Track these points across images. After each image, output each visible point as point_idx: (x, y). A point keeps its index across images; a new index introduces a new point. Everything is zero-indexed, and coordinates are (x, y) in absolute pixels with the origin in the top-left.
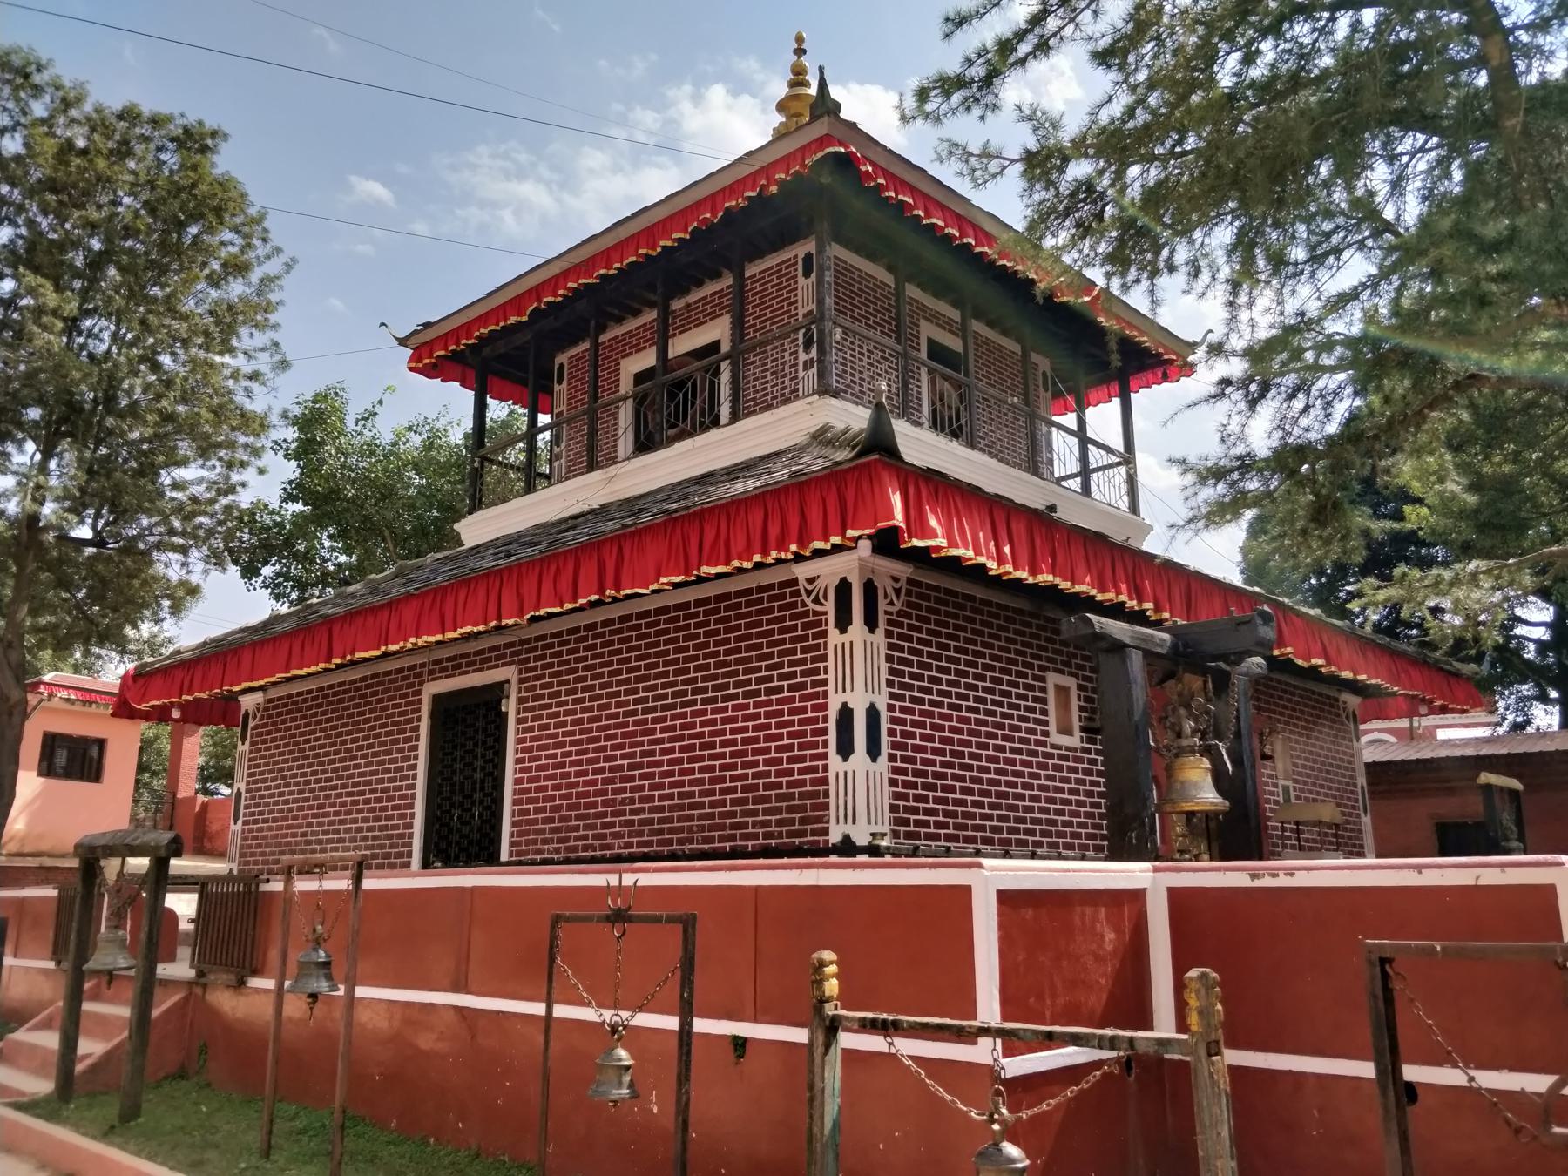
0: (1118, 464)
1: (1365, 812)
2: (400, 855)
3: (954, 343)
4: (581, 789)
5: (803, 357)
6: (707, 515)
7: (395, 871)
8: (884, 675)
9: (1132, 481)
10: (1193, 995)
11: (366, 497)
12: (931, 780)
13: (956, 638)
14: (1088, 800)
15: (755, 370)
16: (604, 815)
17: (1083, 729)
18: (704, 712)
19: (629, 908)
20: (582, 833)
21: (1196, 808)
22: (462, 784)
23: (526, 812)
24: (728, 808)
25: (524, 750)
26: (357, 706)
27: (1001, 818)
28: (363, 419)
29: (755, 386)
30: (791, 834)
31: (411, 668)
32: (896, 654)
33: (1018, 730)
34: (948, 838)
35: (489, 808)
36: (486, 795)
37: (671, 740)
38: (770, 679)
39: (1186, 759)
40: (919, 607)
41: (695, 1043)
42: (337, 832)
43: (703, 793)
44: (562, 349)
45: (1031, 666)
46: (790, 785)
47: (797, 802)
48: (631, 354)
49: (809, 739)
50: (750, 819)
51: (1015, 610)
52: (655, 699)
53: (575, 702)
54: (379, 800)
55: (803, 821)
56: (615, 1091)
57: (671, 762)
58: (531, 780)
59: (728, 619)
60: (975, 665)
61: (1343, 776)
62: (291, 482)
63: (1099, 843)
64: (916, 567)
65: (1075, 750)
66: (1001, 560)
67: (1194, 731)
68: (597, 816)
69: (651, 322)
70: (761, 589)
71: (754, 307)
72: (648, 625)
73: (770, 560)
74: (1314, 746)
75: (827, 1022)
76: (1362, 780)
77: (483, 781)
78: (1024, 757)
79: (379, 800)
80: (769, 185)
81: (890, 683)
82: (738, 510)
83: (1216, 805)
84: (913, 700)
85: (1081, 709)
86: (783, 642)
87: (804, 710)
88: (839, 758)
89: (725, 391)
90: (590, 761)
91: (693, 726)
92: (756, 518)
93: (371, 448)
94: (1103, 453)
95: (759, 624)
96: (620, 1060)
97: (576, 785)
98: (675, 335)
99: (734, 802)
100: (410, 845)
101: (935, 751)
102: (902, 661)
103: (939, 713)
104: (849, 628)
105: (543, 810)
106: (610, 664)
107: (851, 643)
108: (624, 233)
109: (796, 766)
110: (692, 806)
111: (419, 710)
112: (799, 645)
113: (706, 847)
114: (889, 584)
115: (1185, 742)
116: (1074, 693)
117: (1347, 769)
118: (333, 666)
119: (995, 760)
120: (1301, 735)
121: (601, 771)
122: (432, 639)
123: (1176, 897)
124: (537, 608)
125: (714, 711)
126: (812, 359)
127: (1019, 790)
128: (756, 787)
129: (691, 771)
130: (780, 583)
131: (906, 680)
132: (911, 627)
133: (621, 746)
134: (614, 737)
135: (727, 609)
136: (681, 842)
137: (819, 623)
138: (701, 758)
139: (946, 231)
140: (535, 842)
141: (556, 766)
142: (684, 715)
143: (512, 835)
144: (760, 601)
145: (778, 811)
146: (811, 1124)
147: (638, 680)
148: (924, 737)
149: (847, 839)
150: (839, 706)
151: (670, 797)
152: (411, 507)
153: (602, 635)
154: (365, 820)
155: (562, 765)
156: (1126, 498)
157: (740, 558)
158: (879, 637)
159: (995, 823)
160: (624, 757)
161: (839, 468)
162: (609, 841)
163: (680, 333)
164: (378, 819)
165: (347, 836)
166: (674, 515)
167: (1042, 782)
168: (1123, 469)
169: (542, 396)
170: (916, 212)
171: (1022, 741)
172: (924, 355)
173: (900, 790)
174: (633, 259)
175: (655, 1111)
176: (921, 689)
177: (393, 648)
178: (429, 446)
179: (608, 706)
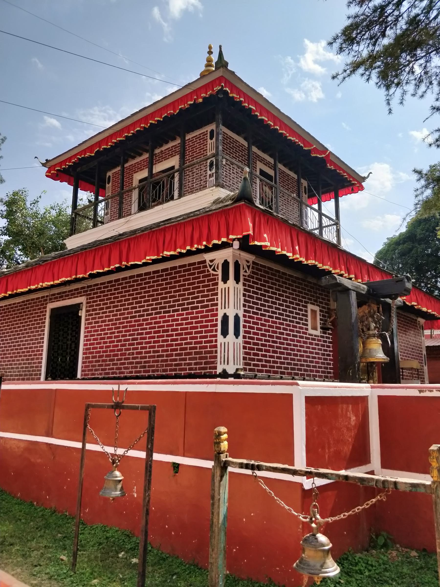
0: (333, 225)
1: (425, 365)
2: (36, 375)
3: (271, 172)
4: (111, 349)
5: (209, 172)
6: (167, 229)
7: (34, 381)
8: (242, 302)
9: (338, 231)
10: (435, 460)
11: (33, 234)
12: (260, 347)
13: (272, 288)
14: (323, 357)
15: (189, 178)
16: (121, 359)
17: (321, 328)
18: (165, 317)
19: (123, 402)
20: (111, 367)
21: (376, 361)
22: (62, 346)
23: (88, 358)
24: (174, 357)
25: (88, 332)
26: (21, 313)
27: (288, 364)
28: (33, 203)
29: (189, 180)
30: (200, 369)
31: (43, 297)
32: (247, 293)
33: (296, 327)
34: (267, 371)
35: (73, 356)
36: (72, 350)
37: (150, 328)
38: (193, 303)
39: (371, 340)
40: (257, 274)
41: (154, 465)
42: (11, 365)
43: (163, 351)
44: (110, 170)
45: (301, 301)
46: (201, 348)
47: (203, 355)
48: (138, 171)
49: (209, 328)
50: (183, 362)
51: (296, 278)
52: (144, 311)
53: (110, 312)
54: (28, 352)
55: (206, 363)
56: (113, 493)
57: (150, 338)
58: (91, 344)
59: (175, 277)
60: (279, 300)
61: (418, 350)
62: (4, 228)
63: (326, 375)
64: (256, 257)
65: (318, 336)
66: (294, 253)
67: (375, 328)
68: (118, 360)
69: (146, 158)
70: (190, 265)
71: (189, 152)
72: (141, 280)
73: (194, 249)
74: (408, 338)
75: (222, 464)
76: (424, 352)
77: (71, 345)
78: (298, 339)
79: (28, 352)
80: (197, 99)
81: (244, 306)
82: (180, 228)
83: (384, 359)
84: (254, 313)
85: (321, 320)
86: (199, 287)
87: (207, 316)
88: (222, 337)
89: (176, 185)
90: (115, 337)
91: (159, 322)
92: (189, 230)
93: (35, 215)
94: (328, 219)
95: (189, 279)
96: (116, 477)
97: (109, 347)
98: (156, 164)
99: (176, 355)
100: (40, 370)
101: (262, 335)
102: (249, 296)
103: (264, 319)
104: (228, 281)
105: (95, 357)
106: (125, 296)
107: (229, 288)
108: (136, 118)
109: (203, 340)
110: (158, 356)
111: (45, 315)
112: (206, 289)
113: (164, 373)
114: (245, 263)
115: (371, 332)
116: (318, 313)
117: (419, 348)
118: (7, 295)
119: (286, 339)
120: (403, 333)
121: (120, 341)
122: (49, 284)
123: (381, 398)
124: (93, 270)
125: (169, 316)
126: (213, 174)
127: (296, 352)
128: (186, 349)
129: (158, 342)
130: (198, 262)
131: (251, 305)
132: (254, 282)
133: (129, 331)
134: (126, 327)
135: (175, 273)
136: (153, 371)
137: (215, 279)
138: (163, 336)
139: (268, 122)
140: (91, 370)
141: (101, 339)
142: (156, 318)
143: (82, 367)
144: (190, 270)
145: (195, 359)
146: (212, 517)
147: (137, 303)
148: (258, 329)
149: (224, 371)
150: (223, 315)
151: (149, 352)
152: (51, 239)
153: (122, 284)
154: (23, 360)
155: (104, 338)
156: (336, 238)
157: (181, 248)
158: (240, 286)
159: (286, 366)
160: (130, 335)
161: (226, 208)
162: (123, 370)
163: (158, 163)
164: (28, 360)
165: (15, 366)
166: (153, 230)
167: (305, 349)
168: (335, 227)
169: (101, 190)
170: (256, 113)
171: (297, 332)
172: (258, 173)
173: (247, 351)
174: (139, 129)
175: (135, 496)
176: (257, 309)
177: (33, 287)
178: (59, 214)
179: (124, 314)
